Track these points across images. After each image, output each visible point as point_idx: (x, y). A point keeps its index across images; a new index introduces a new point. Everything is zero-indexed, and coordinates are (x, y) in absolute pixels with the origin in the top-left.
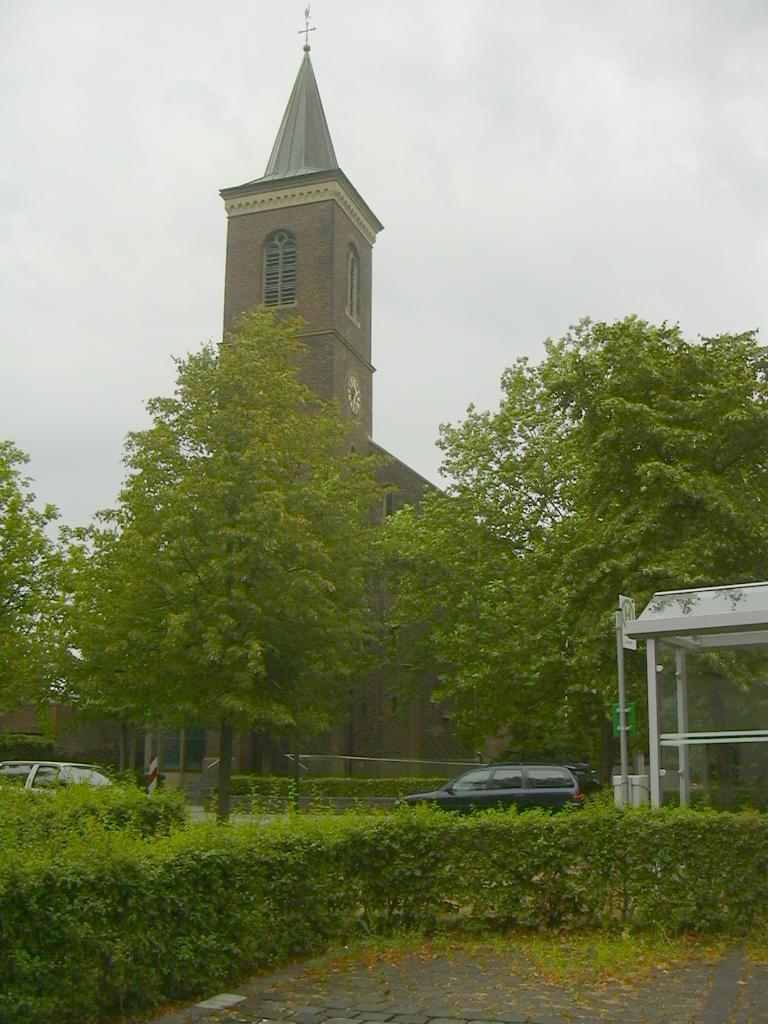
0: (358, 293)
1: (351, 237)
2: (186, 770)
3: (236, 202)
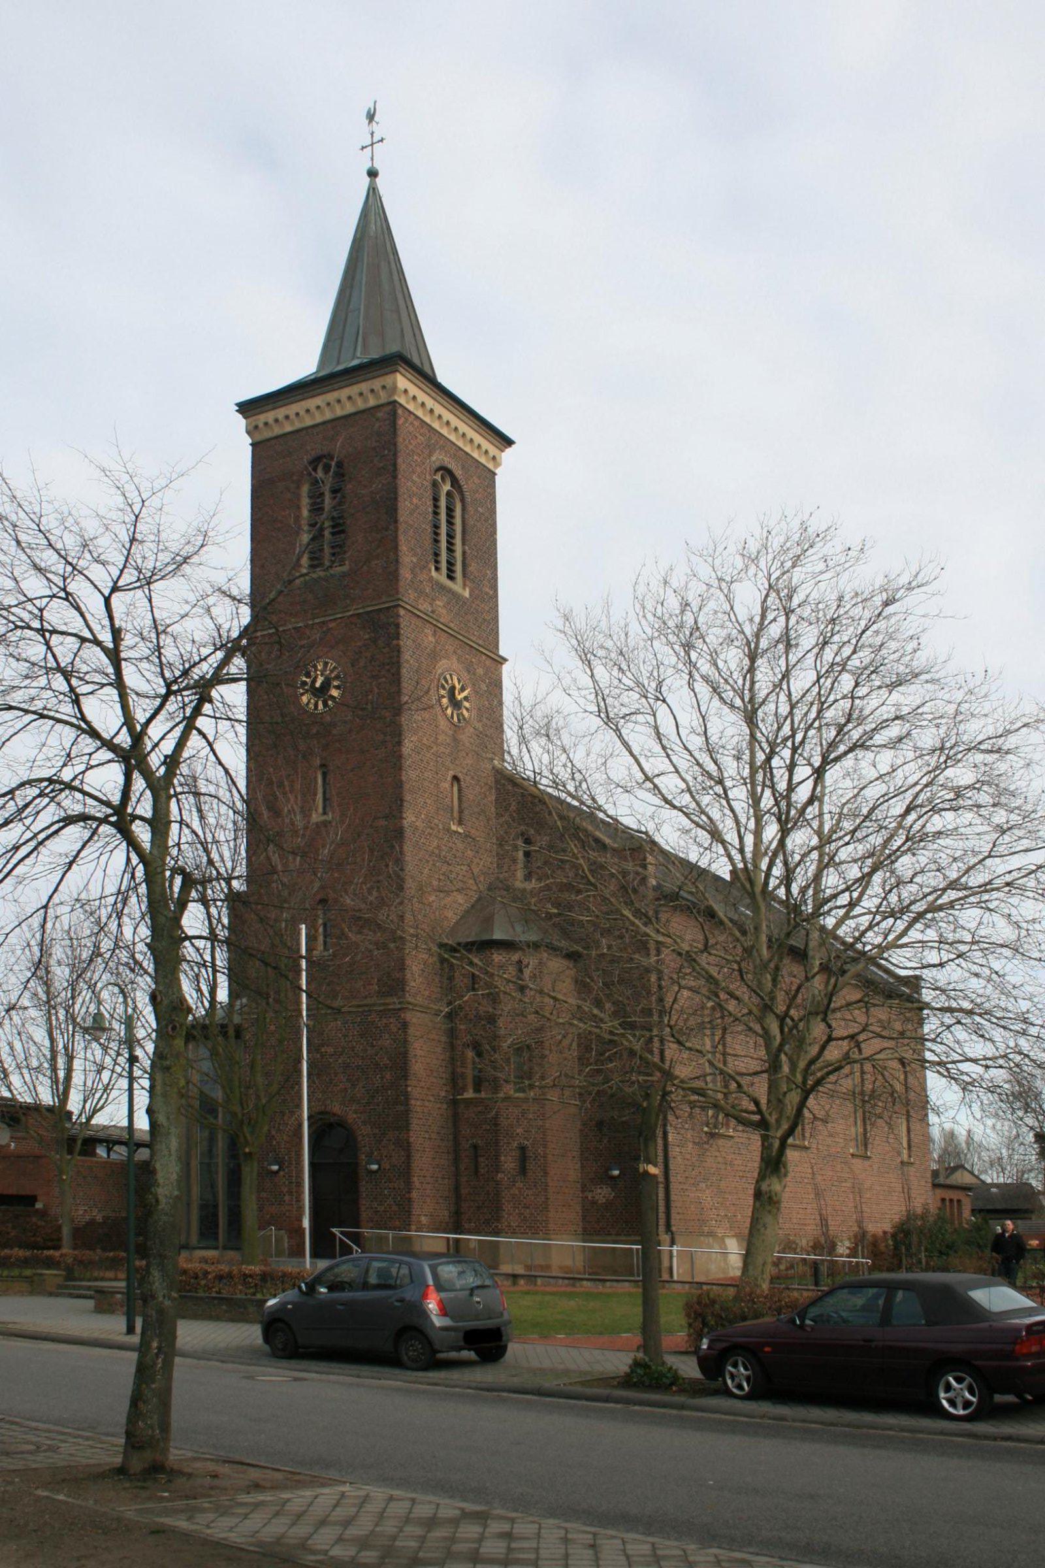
0: (464, 544)
1: (438, 458)
2: (225, 1248)
3: (262, 418)
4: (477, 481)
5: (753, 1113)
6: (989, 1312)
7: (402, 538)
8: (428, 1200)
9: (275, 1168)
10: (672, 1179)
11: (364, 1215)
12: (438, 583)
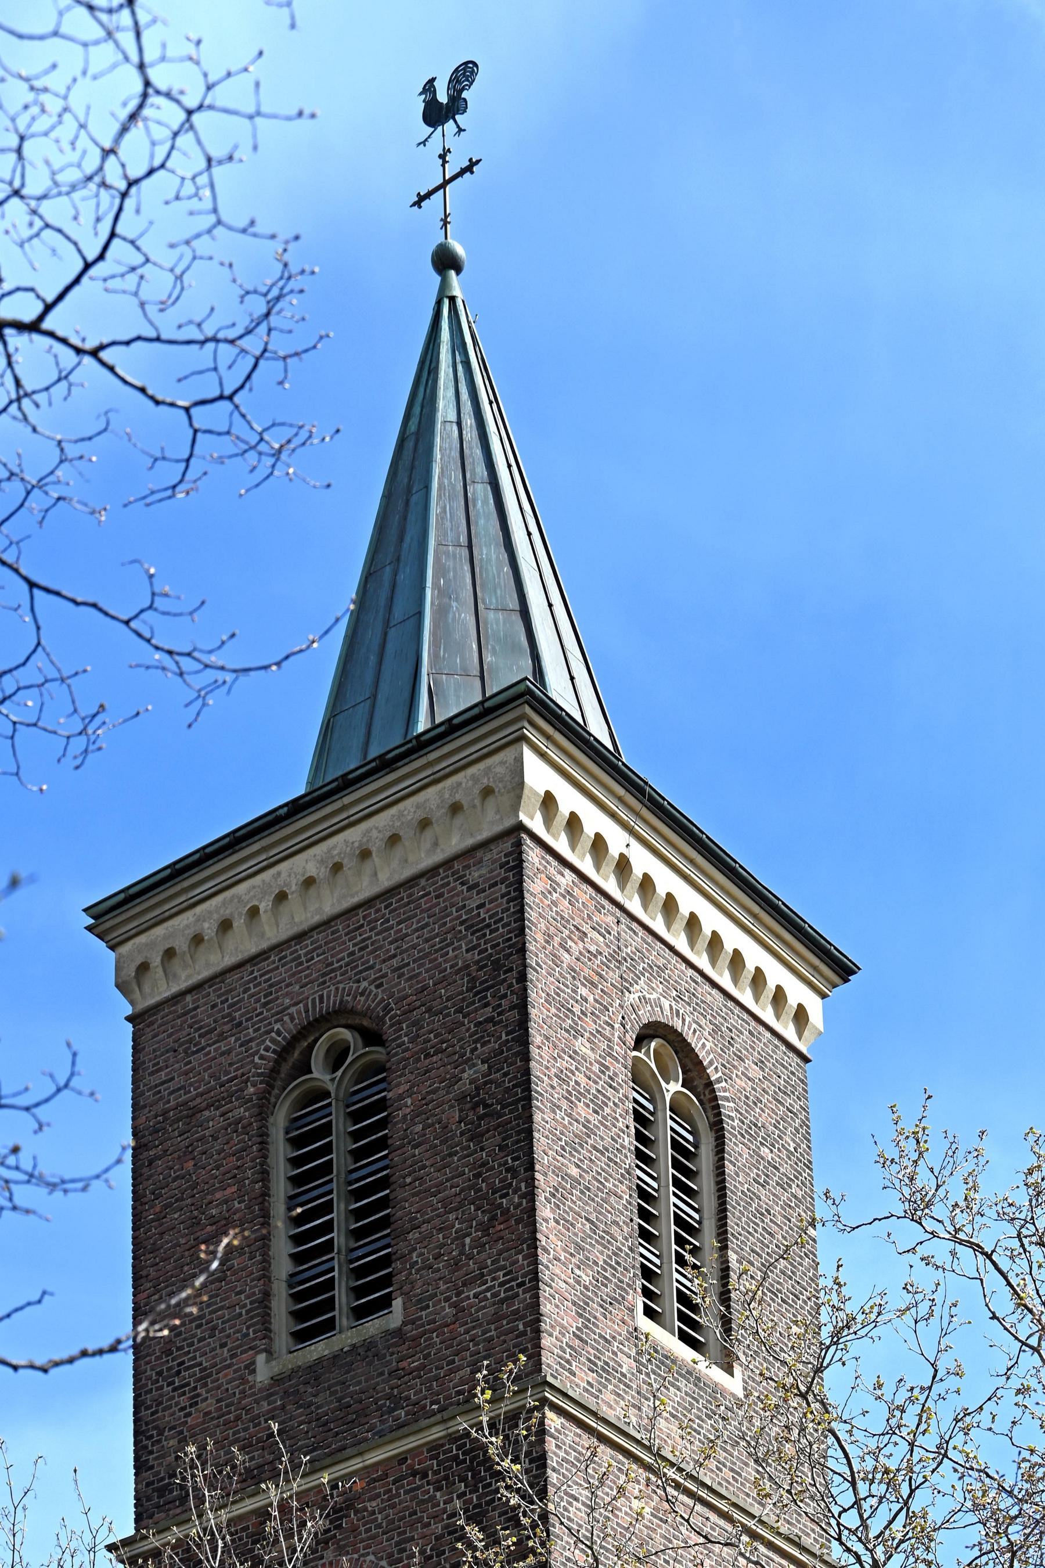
4: (755, 1072)
7: (545, 1211)
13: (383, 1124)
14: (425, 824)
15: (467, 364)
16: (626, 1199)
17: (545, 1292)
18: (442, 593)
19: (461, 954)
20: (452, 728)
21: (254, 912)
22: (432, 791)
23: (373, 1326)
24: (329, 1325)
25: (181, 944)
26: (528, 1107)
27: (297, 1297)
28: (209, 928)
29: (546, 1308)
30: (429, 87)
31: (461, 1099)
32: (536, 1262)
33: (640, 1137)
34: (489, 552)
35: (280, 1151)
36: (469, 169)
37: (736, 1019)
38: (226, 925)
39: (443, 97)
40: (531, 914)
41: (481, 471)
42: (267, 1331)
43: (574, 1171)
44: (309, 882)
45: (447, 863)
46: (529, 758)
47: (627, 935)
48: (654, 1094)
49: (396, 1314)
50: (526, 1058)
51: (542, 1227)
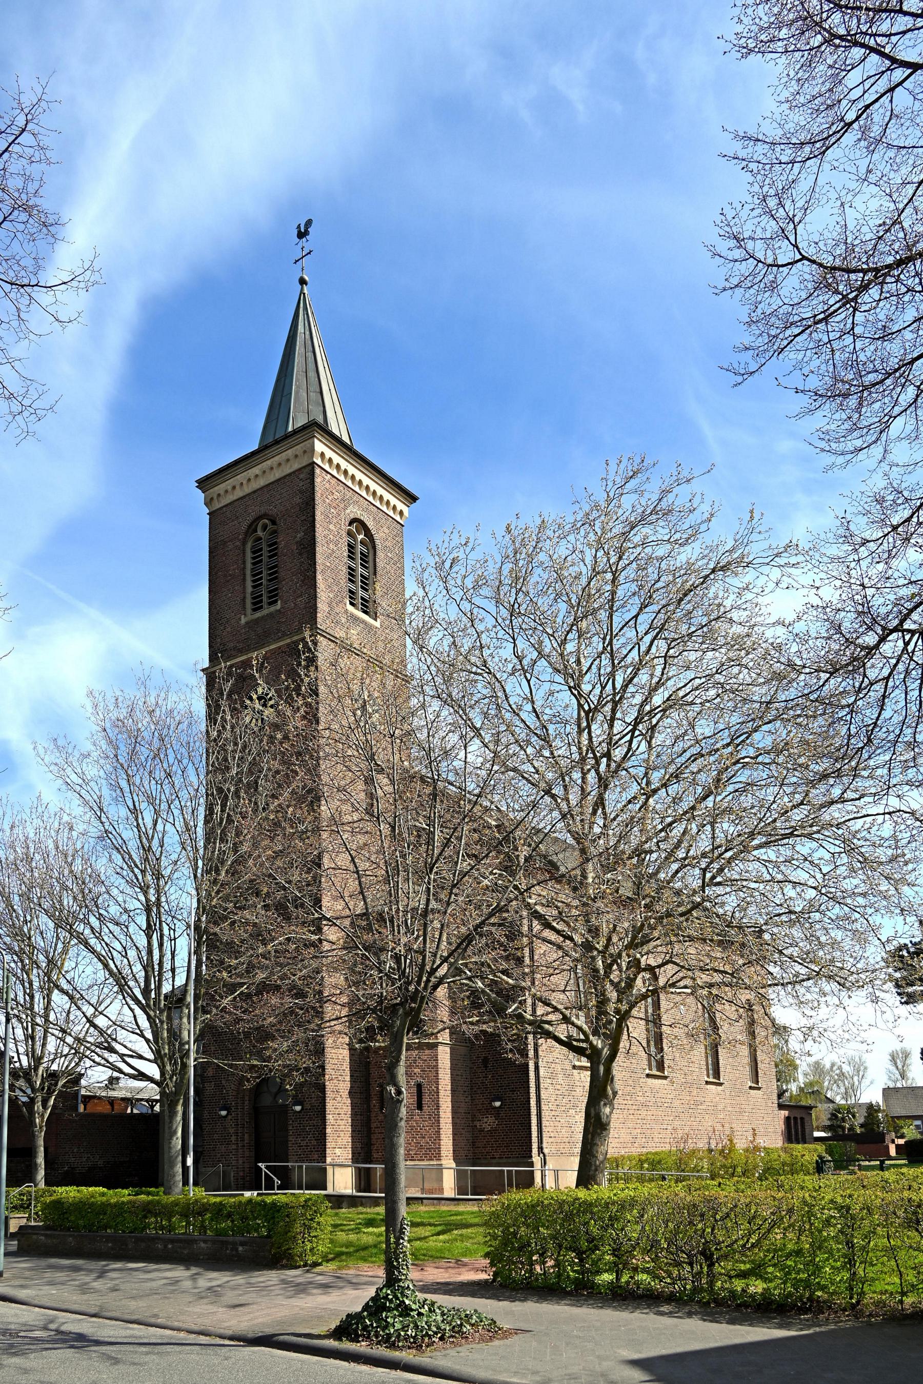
1: (354, 511)
4: (387, 531)
5: (583, 1041)
6: (533, 1295)
7: (319, 577)
8: (342, 1134)
9: (224, 1113)
10: (543, 1107)
11: (292, 1149)
12: (352, 615)
13: (276, 549)
14: (288, 460)
15: (307, 314)
16: (345, 570)
17: (318, 600)
18: (298, 387)
19: (297, 500)
20: (295, 432)
21: (242, 484)
22: (290, 451)
23: (272, 609)
24: (261, 607)
25: (222, 493)
26: (315, 546)
27: (253, 598)
28: (229, 488)
29: (319, 605)
30: (299, 226)
31: (297, 543)
32: (316, 592)
33: (349, 551)
34: (312, 374)
35: (249, 555)
36: (309, 253)
37: (381, 514)
38: (234, 488)
39: (303, 230)
40: (317, 489)
41: (311, 348)
42: (244, 608)
43: (328, 564)
44: (257, 476)
45: (294, 472)
46: (316, 441)
47: (347, 493)
48: (355, 539)
49: (278, 606)
50: (314, 531)
51: (318, 581)
